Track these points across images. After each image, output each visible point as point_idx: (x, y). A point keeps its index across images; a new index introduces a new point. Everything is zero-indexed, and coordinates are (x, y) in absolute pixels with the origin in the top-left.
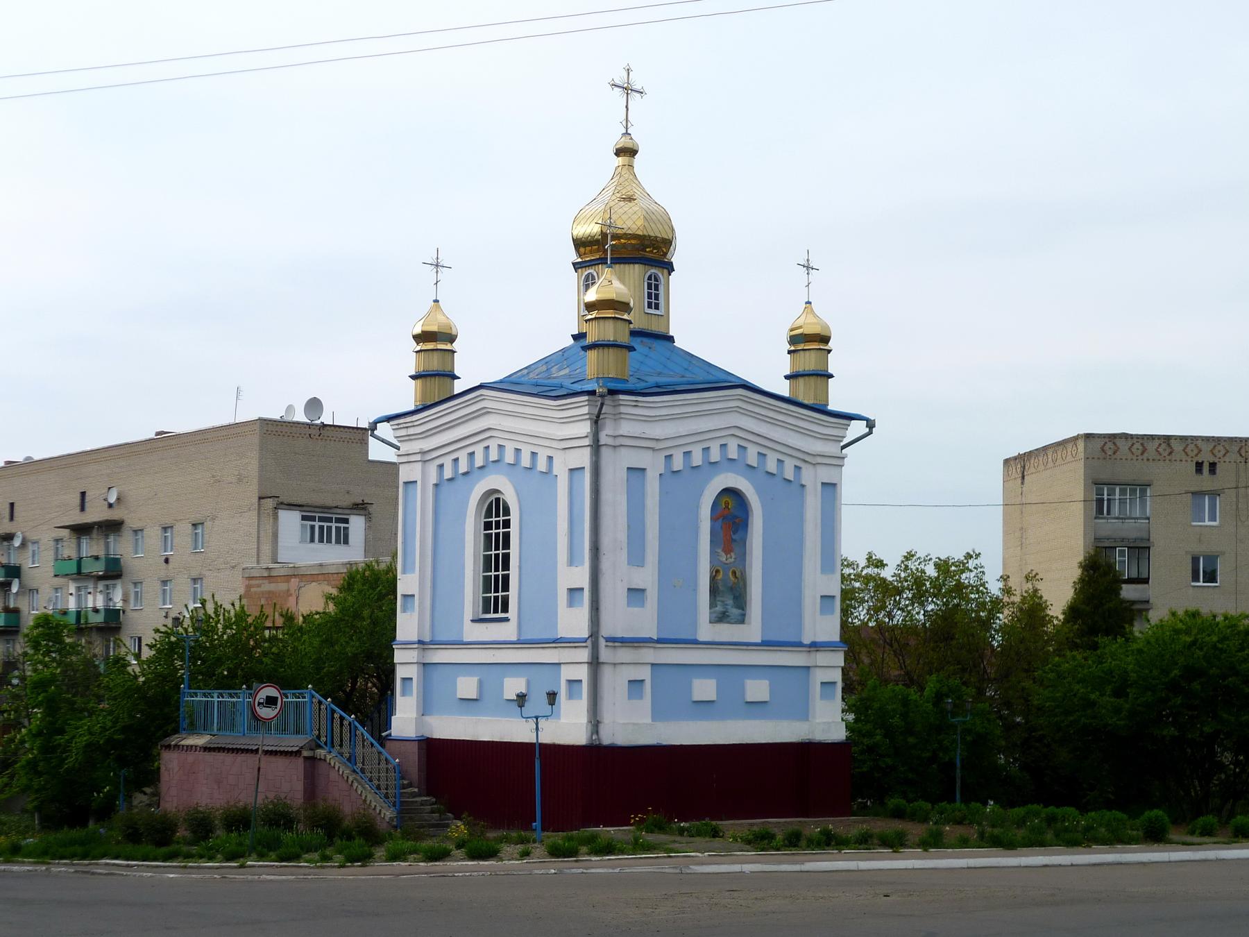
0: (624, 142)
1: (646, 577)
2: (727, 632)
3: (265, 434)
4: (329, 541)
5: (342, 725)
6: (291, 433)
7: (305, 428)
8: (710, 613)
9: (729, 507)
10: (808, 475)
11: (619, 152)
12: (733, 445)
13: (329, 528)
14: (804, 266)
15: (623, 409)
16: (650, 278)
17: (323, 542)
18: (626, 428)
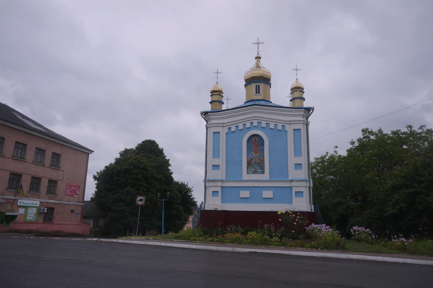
9: (257, 140)
10: (287, 128)
11: (256, 58)
15: (210, 117)
16: (257, 86)
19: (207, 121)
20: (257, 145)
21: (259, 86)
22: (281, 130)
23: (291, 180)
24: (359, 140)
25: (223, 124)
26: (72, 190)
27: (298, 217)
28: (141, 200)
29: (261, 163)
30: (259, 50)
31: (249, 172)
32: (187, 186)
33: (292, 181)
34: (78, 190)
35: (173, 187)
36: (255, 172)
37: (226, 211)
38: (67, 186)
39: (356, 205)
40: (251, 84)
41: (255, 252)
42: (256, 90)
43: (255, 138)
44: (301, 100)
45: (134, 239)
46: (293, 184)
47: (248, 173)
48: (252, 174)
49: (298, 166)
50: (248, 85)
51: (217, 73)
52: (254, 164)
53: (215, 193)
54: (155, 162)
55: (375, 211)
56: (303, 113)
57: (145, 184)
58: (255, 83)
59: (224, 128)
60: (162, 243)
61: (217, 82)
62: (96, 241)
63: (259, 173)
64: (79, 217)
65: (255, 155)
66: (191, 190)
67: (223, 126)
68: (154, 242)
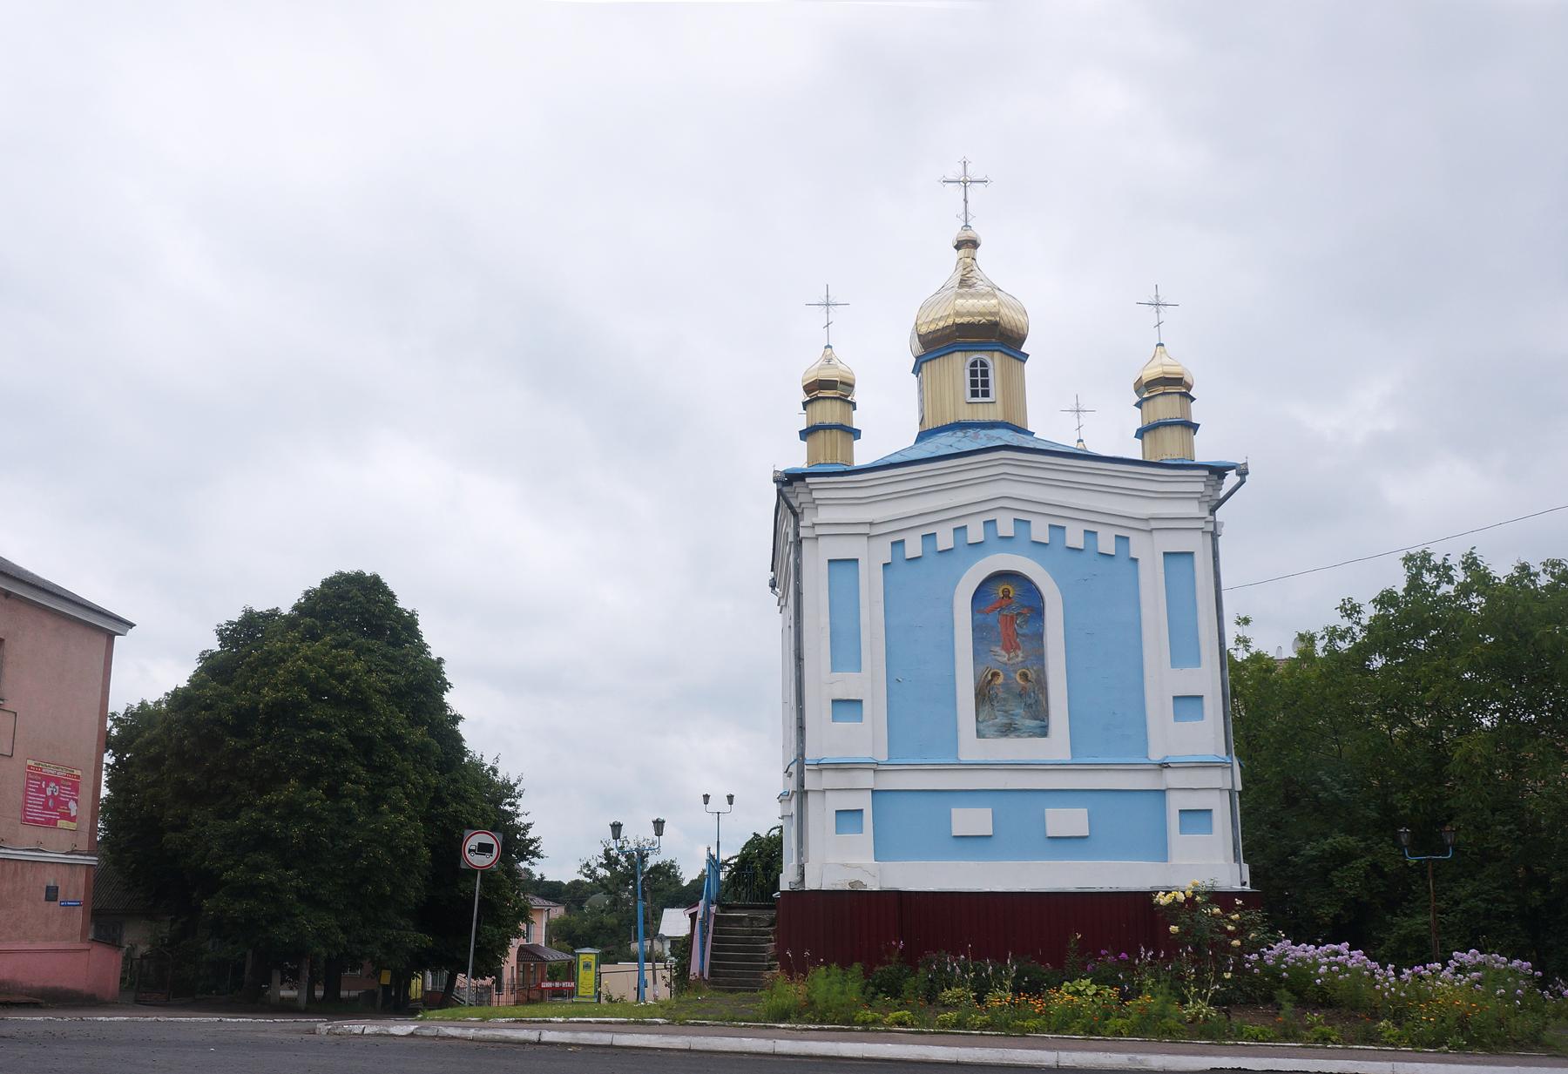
0: (965, 236)
1: (868, 682)
10: (1139, 546)
15: (815, 495)
16: (974, 364)
18: (825, 515)
19: (798, 510)
20: (1012, 617)
21: (983, 364)
22: (1113, 556)
23: (1160, 765)
24: (1387, 599)
25: (871, 524)
26: (47, 798)
27: (1237, 916)
28: (484, 849)
29: (1034, 692)
30: (969, 210)
31: (982, 728)
32: (495, 774)
33: (1166, 767)
34: (74, 799)
35: (464, 777)
36: (1008, 730)
37: (899, 894)
38: (28, 779)
39: (1415, 861)
40: (950, 356)
41: (1239, 1068)
42: (974, 383)
43: (1006, 587)
44: (1184, 430)
45: (564, 1022)
46: (1171, 779)
47: (980, 734)
48: (996, 737)
49: (1187, 704)
50: (935, 358)
51: (828, 305)
53: (849, 817)
54: (391, 672)
55: (1495, 885)
56: (1200, 487)
57: (362, 772)
58: (968, 353)
59: (874, 542)
60: (777, 1041)
61: (829, 346)
62: (412, 1035)
63: (1026, 735)
64: (78, 917)
66: (512, 788)
68: (833, 1041)
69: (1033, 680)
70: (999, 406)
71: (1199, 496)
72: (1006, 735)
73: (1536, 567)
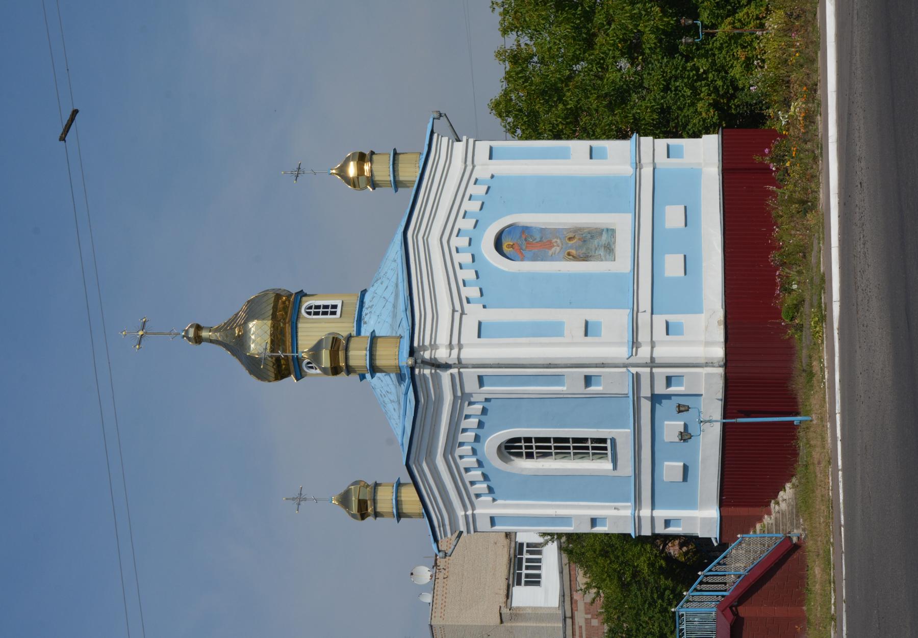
1: (573, 318)
2: (623, 245)
3: (444, 619)
4: (539, 561)
5: (707, 583)
6: (443, 595)
7: (438, 583)
8: (606, 260)
9: (512, 244)
12: (456, 242)
13: (528, 560)
14: (297, 176)
15: (427, 343)
16: (309, 313)
17: (540, 566)
18: (443, 338)
20: (528, 243)
52: (585, 249)
65: (558, 249)
67: (460, 311)
69: (574, 234)
70: (346, 299)
71: (451, 141)
72: (613, 250)
73: (511, 41)
